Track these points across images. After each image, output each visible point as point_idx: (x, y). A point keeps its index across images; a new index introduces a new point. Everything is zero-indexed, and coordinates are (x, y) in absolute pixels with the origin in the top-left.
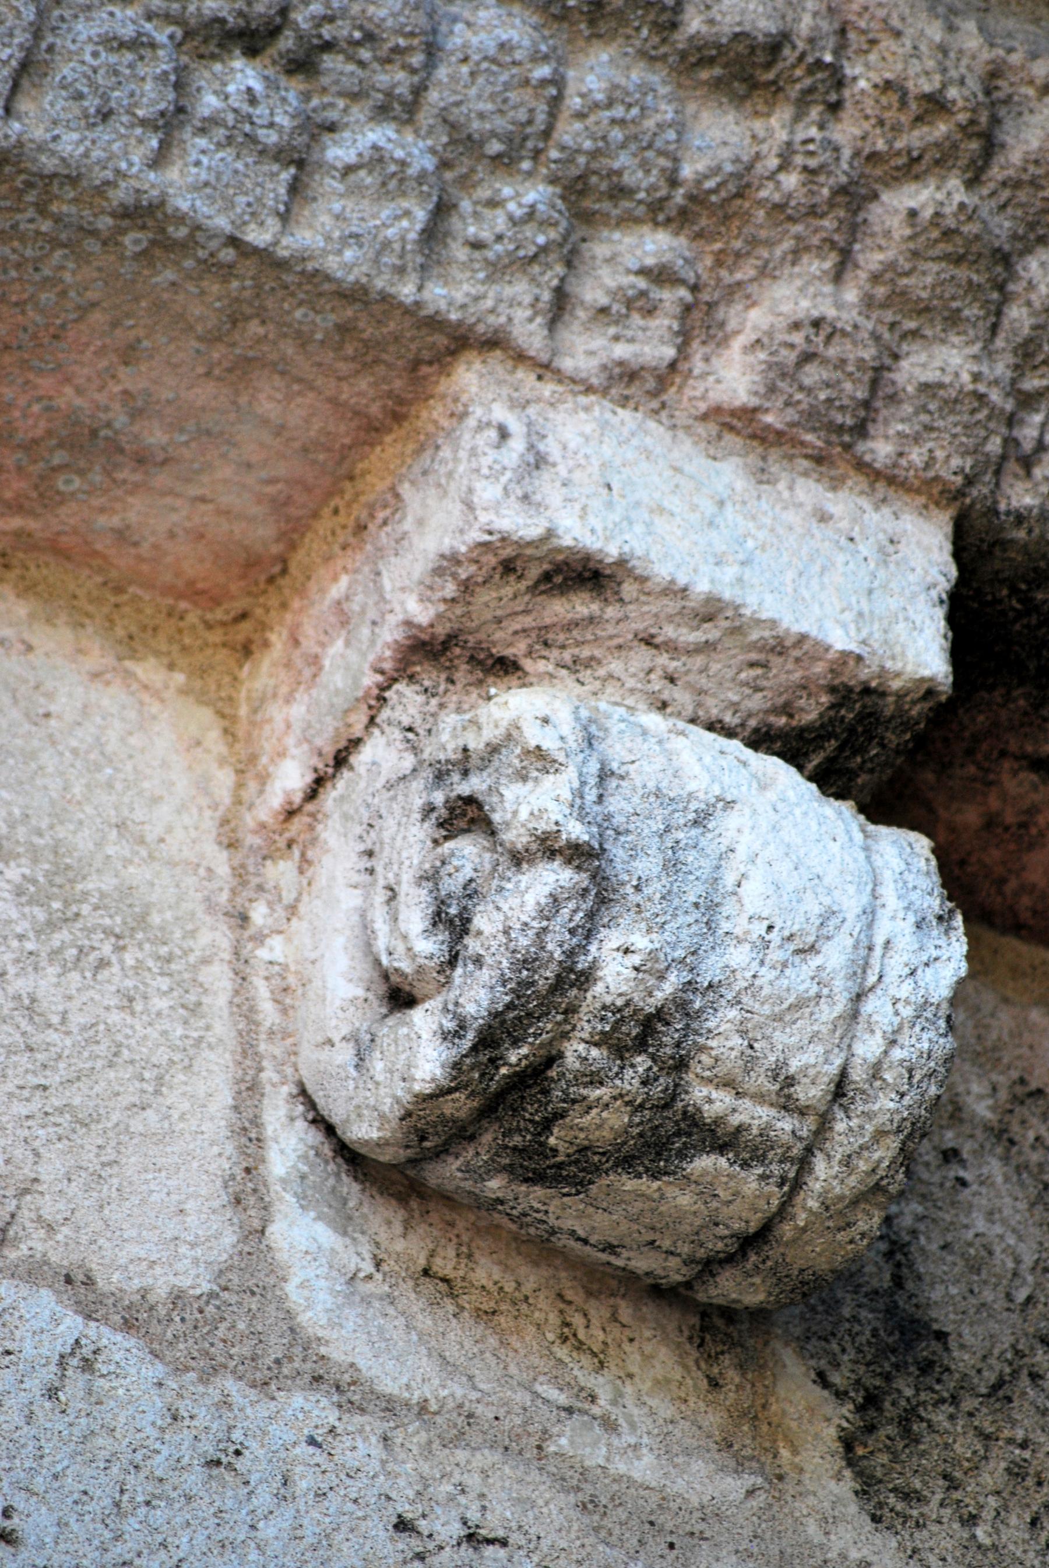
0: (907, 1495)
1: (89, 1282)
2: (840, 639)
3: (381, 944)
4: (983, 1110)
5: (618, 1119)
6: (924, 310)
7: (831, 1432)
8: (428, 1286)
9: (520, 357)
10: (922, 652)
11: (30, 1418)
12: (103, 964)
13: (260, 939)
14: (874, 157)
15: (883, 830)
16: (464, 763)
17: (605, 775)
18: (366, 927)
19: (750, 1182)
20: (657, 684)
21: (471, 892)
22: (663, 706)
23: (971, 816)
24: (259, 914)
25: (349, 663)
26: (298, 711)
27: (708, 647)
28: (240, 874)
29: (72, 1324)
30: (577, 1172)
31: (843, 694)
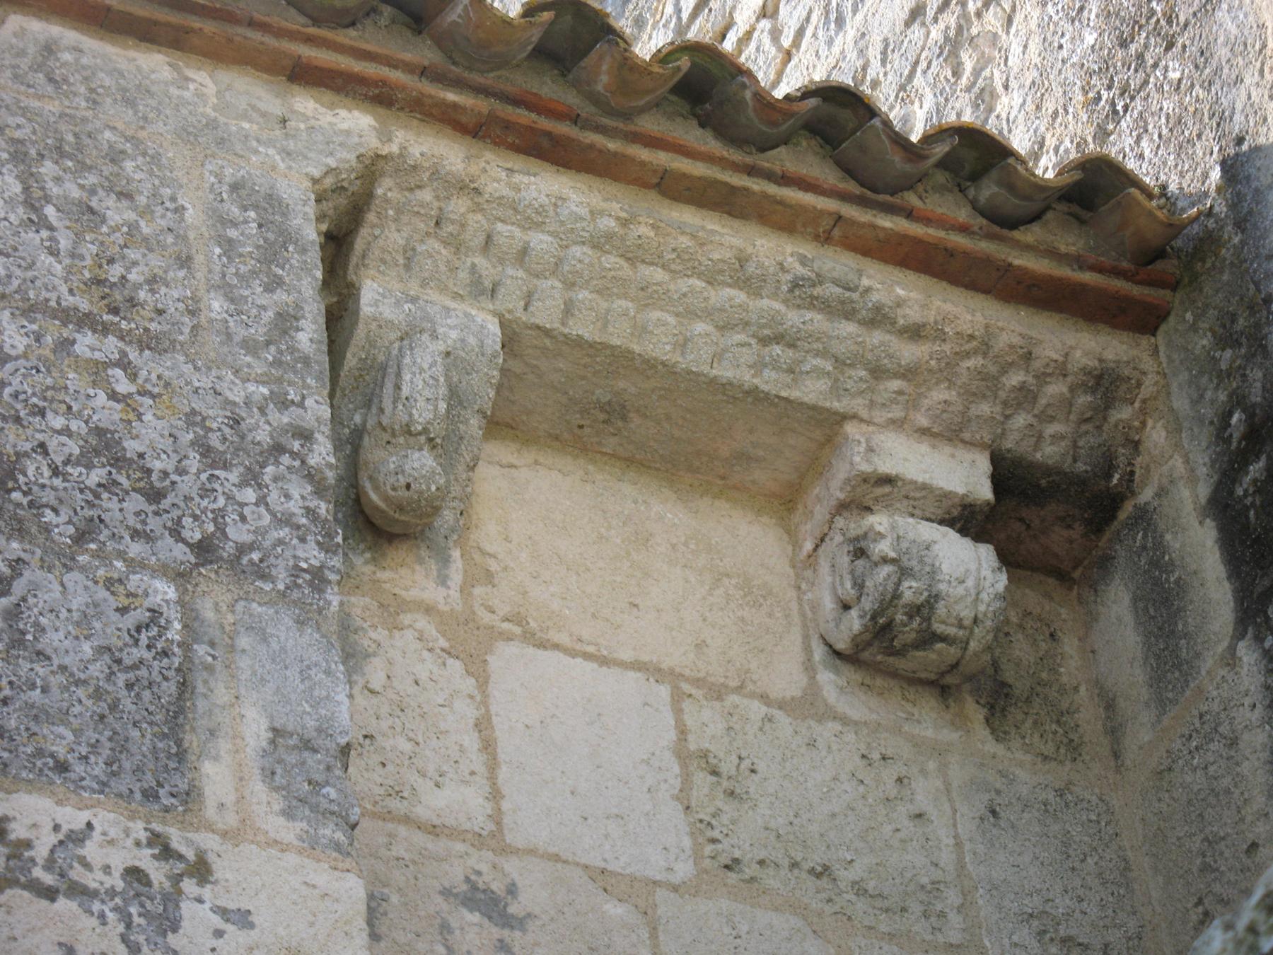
0: (1005, 733)
1: (768, 697)
2: (961, 490)
3: (840, 592)
4: (1015, 620)
5: (913, 635)
6: (974, 394)
7: (981, 717)
8: (863, 688)
9: (862, 420)
10: (985, 492)
11: (755, 737)
12: (761, 605)
13: (804, 593)
14: (956, 353)
15: (979, 545)
16: (857, 539)
17: (898, 537)
18: (834, 588)
19: (952, 650)
20: (911, 509)
21: (863, 574)
22: (912, 515)
23: (1002, 536)
24: (804, 586)
25: (821, 513)
26: (808, 527)
27: (924, 497)
28: (797, 575)
29: (764, 709)
30: (900, 653)
31: (965, 507)
